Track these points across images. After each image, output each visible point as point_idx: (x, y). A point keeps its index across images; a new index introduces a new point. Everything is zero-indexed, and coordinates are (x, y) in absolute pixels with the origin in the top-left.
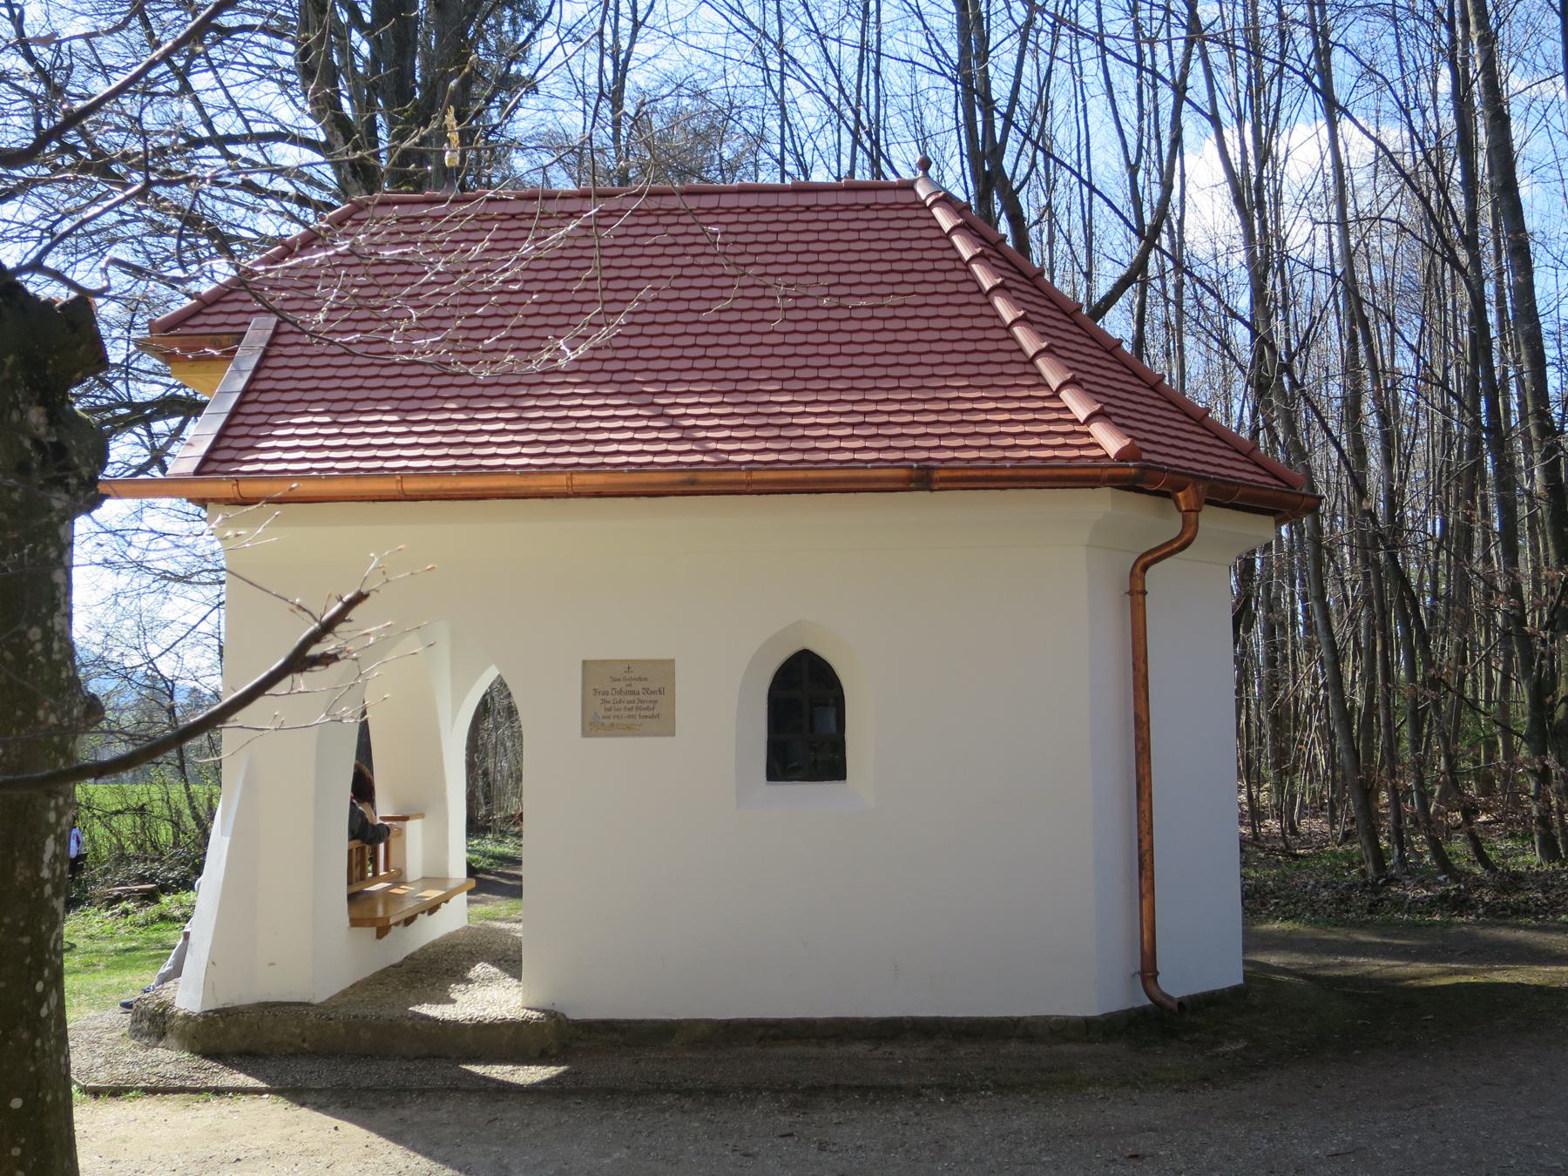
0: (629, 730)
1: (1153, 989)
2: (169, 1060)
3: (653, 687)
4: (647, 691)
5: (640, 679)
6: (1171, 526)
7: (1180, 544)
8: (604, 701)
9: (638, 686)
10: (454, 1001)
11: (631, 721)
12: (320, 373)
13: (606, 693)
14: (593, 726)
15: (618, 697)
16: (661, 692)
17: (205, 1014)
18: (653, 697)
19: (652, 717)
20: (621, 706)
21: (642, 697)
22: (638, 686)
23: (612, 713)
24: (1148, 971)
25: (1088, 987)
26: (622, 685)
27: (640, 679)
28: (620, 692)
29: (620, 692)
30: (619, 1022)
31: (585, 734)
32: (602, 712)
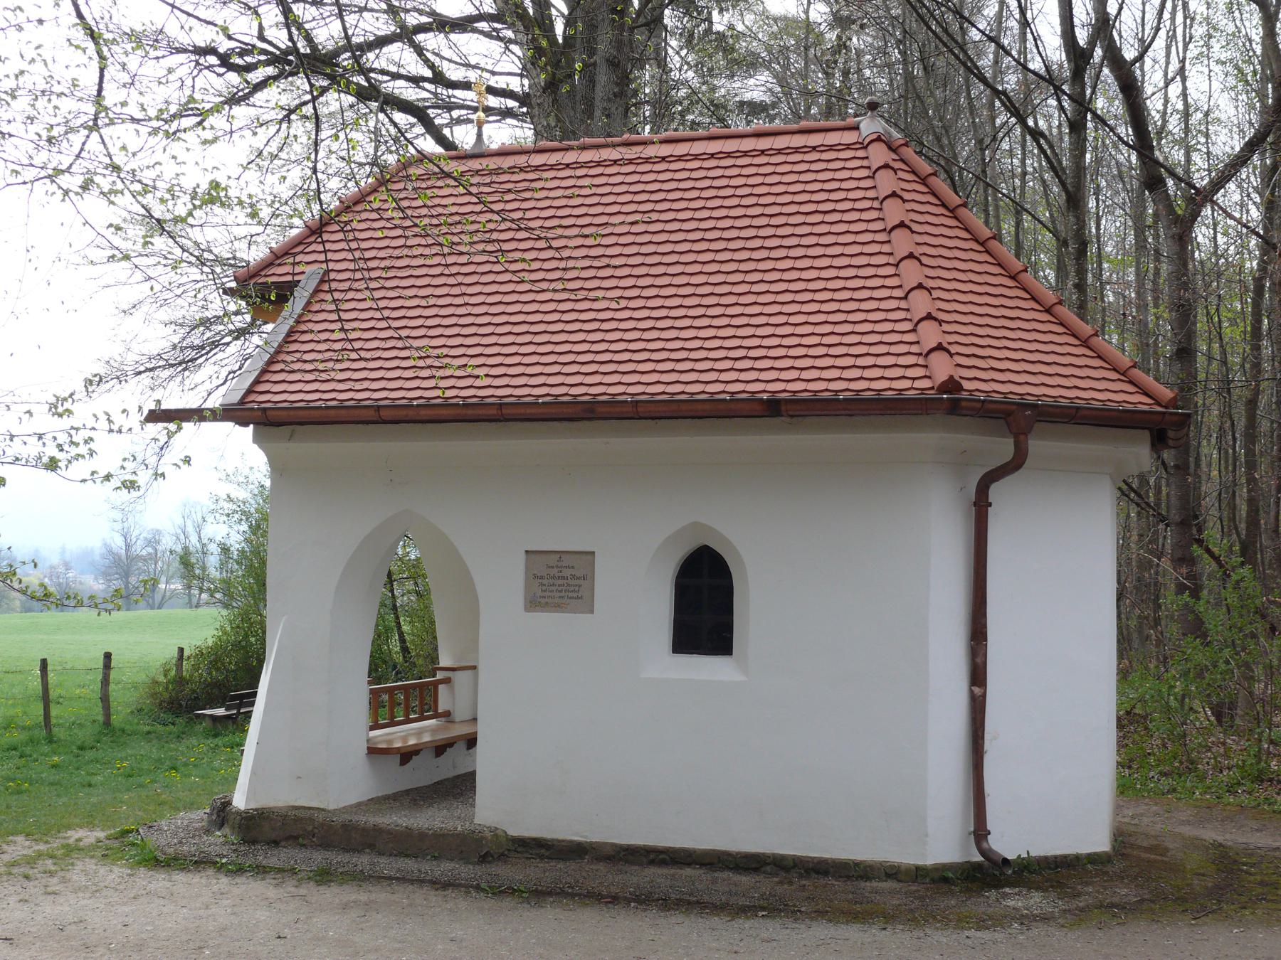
0: (558, 607)
1: (985, 845)
2: (217, 842)
3: (578, 575)
4: (574, 577)
5: (568, 567)
6: (1004, 448)
7: (1016, 464)
8: (541, 584)
9: (567, 572)
10: (42, 585)
11: (560, 601)
12: (655, 314)
13: (542, 578)
14: (534, 603)
15: (551, 581)
16: (584, 578)
17: (246, 812)
18: (577, 582)
19: (578, 598)
20: (554, 588)
21: (570, 581)
22: (567, 572)
23: (547, 594)
24: (980, 832)
25: (944, 845)
26: (554, 572)
27: (568, 567)
28: (553, 577)
29: (553, 577)
30: (545, 840)
31: (527, 610)
32: (539, 593)
